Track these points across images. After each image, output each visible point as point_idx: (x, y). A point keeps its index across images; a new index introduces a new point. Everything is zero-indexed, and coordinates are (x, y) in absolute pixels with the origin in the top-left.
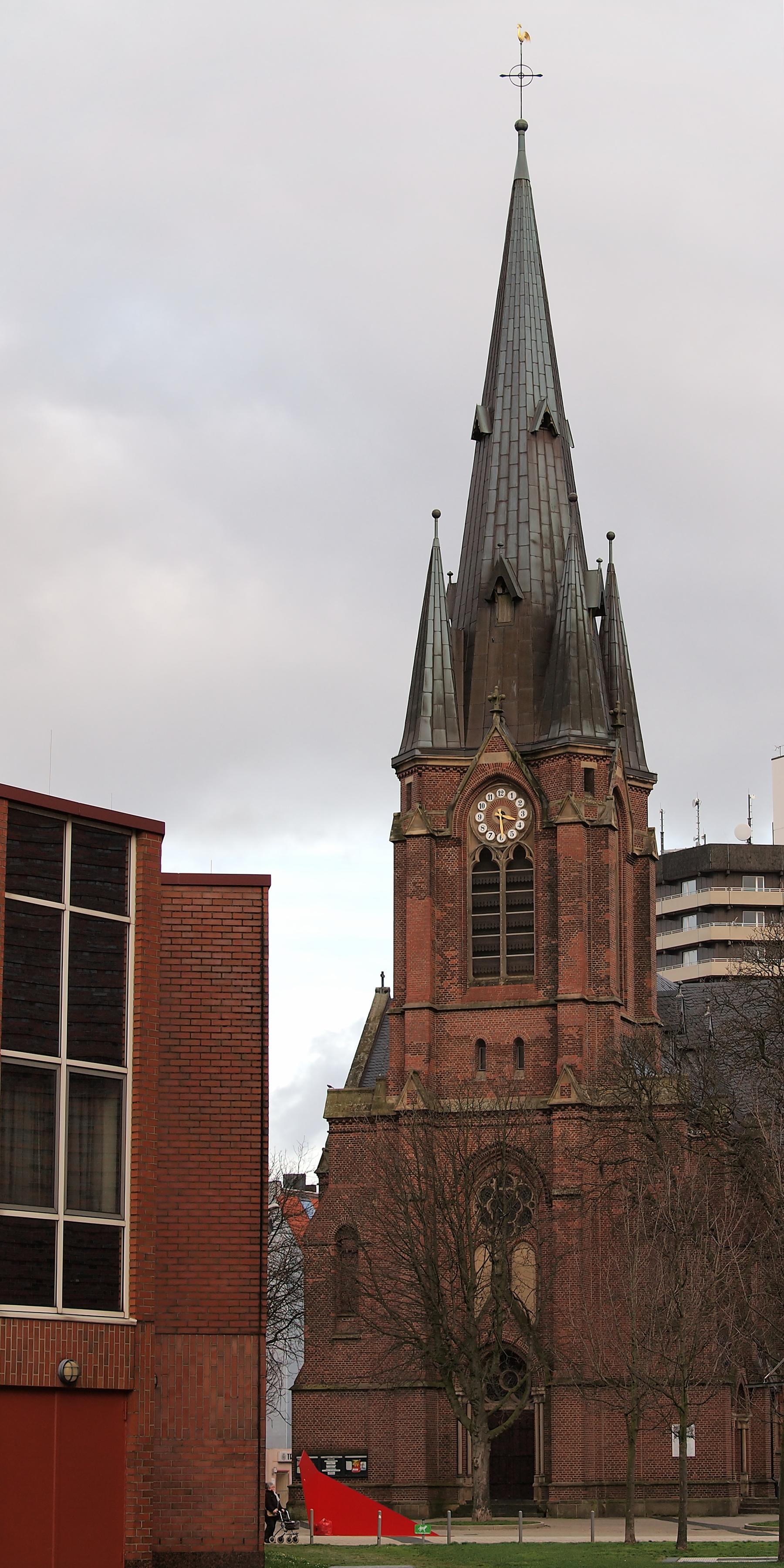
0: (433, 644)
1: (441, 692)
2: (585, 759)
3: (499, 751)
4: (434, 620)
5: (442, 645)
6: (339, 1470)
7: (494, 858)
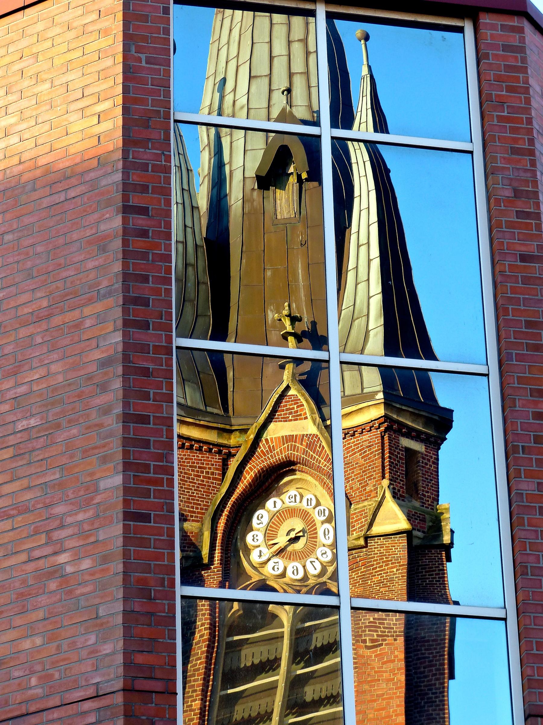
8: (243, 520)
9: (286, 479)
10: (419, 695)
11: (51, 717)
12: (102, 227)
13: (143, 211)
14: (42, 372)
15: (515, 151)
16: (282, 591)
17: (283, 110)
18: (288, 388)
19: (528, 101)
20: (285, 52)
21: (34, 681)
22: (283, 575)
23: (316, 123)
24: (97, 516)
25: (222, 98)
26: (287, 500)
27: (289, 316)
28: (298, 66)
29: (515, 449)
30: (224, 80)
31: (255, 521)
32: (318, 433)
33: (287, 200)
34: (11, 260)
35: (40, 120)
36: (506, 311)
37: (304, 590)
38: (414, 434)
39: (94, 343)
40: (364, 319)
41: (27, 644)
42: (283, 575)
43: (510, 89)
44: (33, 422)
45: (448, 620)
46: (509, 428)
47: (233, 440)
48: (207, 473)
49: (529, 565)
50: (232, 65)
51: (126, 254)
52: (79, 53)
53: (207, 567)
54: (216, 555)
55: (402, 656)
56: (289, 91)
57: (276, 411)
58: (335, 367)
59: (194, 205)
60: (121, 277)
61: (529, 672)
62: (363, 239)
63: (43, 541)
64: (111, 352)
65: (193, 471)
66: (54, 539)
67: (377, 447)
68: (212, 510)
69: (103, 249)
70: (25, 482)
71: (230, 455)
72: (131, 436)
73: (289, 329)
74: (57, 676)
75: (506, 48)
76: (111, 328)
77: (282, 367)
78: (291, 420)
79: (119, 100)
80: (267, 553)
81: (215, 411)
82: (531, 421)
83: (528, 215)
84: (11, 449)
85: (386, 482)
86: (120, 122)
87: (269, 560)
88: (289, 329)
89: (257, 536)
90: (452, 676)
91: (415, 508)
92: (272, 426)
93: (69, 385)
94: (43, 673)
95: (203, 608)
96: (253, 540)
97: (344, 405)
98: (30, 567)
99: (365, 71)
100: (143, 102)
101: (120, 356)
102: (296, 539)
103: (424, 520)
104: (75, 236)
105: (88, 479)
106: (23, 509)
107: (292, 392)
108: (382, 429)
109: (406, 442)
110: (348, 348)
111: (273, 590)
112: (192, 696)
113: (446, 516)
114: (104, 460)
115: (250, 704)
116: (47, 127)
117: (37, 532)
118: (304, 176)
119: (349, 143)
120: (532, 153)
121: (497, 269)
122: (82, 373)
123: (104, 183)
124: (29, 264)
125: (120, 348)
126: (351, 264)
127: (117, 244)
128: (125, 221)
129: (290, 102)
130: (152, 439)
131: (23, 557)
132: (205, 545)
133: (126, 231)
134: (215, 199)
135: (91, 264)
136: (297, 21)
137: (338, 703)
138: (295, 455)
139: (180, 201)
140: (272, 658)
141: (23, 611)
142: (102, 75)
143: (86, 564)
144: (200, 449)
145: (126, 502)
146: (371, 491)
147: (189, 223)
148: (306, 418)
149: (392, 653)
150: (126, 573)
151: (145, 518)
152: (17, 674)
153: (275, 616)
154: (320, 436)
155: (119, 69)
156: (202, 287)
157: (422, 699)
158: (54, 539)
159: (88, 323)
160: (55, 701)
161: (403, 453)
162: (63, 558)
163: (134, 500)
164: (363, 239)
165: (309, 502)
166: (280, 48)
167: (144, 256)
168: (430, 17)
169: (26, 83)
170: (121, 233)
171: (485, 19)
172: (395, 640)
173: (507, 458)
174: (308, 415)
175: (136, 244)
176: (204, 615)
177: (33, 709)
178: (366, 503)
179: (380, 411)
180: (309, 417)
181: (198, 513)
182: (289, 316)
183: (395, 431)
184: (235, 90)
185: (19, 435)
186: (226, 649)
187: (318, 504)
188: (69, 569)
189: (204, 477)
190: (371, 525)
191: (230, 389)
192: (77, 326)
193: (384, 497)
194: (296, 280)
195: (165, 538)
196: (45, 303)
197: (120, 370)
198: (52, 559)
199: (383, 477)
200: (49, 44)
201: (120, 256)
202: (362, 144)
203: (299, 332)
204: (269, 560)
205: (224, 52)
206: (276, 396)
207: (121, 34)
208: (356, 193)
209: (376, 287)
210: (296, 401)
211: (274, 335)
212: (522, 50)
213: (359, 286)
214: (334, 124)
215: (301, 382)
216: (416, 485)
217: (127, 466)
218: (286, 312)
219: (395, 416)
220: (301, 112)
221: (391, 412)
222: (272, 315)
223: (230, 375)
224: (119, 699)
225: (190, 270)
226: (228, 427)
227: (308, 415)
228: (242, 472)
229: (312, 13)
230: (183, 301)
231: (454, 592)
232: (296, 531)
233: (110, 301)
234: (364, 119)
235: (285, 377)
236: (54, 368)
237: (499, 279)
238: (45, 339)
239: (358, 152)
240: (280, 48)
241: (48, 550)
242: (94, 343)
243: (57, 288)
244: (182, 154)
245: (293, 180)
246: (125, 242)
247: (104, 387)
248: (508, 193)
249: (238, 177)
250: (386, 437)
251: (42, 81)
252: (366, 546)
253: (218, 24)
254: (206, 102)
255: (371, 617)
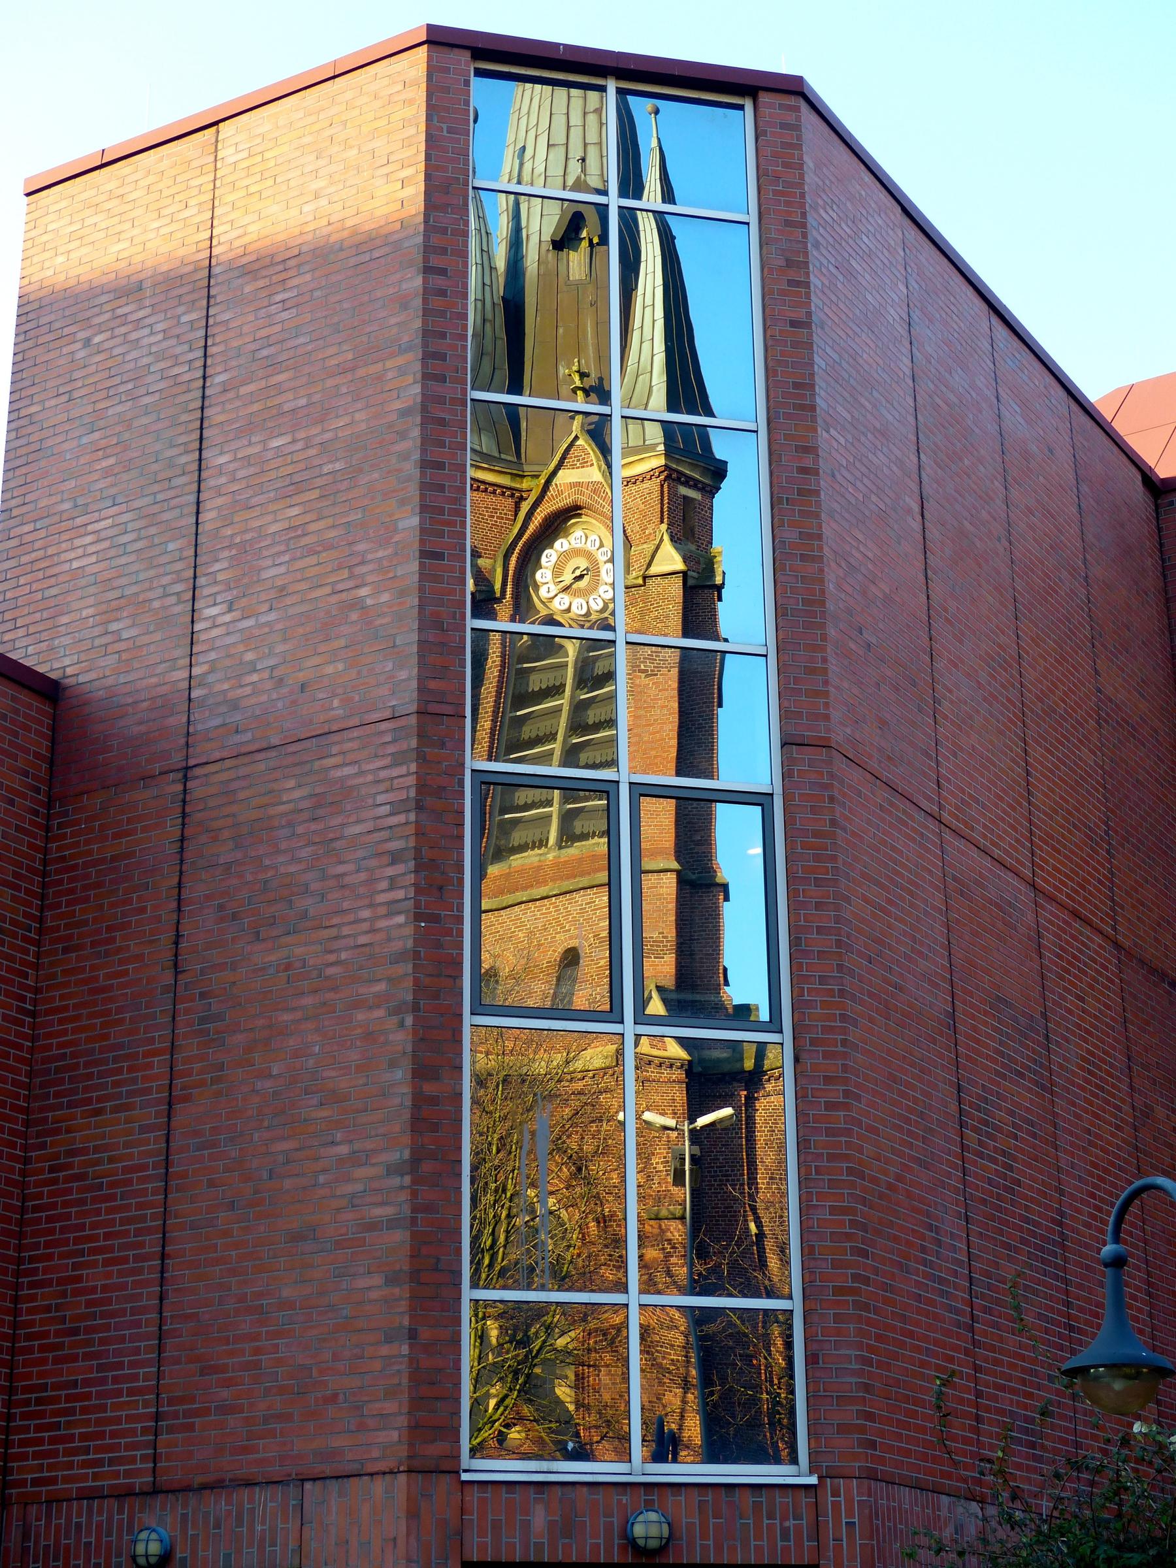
8: (533, 557)
9: (573, 521)
10: (691, 721)
11: (351, 736)
12: (404, 286)
13: (443, 272)
14: (347, 419)
15: (788, 223)
16: (567, 625)
17: (578, 178)
18: (576, 438)
19: (802, 176)
20: (580, 123)
21: (336, 703)
22: (568, 610)
23: (604, 192)
24: (396, 554)
25: (521, 165)
26: (573, 542)
27: (578, 372)
28: (592, 137)
29: (780, 500)
30: (524, 148)
31: (544, 559)
32: (603, 480)
33: (579, 263)
34: (319, 315)
35: (348, 184)
36: (775, 373)
37: (588, 625)
38: (691, 483)
39: (395, 394)
40: (649, 374)
41: (329, 669)
42: (568, 610)
43: (785, 165)
44: (338, 466)
45: (719, 656)
46: (775, 480)
47: (525, 484)
48: (501, 513)
49: (789, 607)
50: (532, 134)
51: (426, 312)
52: (384, 122)
53: (499, 601)
54: (508, 590)
55: (676, 685)
56: (583, 160)
57: (565, 459)
58: (617, 422)
59: (493, 266)
60: (420, 333)
61: (786, 704)
62: (649, 301)
63: (346, 576)
64: (411, 403)
65: (487, 512)
66: (356, 573)
67: (656, 494)
68: (504, 548)
69: (405, 307)
70: (330, 521)
71: (522, 499)
72: (428, 481)
73: (578, 383)
74: (357, 698)
75: (784, 126)
76: (411, 381)
77: (572, 418)
78: (578, 468)
79: (422, 167)
80: (554, 590)
81: (509, 458)
82: (796, 475)
83: (798, 284)
84: (318, 491)
85: (664, 527)
86: (422, 188)
87: (556, 595)
88: (578, 383)
90: (720, 705)
91: (691, 551)
92: (561, 473)
93: (372, 432)
94: (344, 696)
95: (495, 638)
97: (624, 456)
98: (334, 599)
99: (654, 143)
100: (445, 169)
101: (419, 407)
102: (581, 577)
103: (698, 563)
104: (379, 294)
105: (388, 520)
106: (328, 546)
107: (580, 442)
108: (662, 477)
109: (684, 491)
110: (632, 405)
111: (560, 624)
112: (484, 717)
113: (718, 559)
114: (403, 502)
115: (538, 725)
116: (354, 191)
117: (340, 568)
118: (596, 240)
119: (638, 212)
120: (804, 225)
121: (769, 333)
122: (384, 421)
123: (406, 245)
124: (336, 319)
125: (419, 399)
126: (637, 324)
127: (418, 302)
128: (425, 281)
129: (584, 170)
130: (447, 484)
131: (328, 590)
133: (426, 291)
134: (511, 262)
135: (393, 321)
136: (593, 96)
137: (612, 726)
138: (583, 499)
139: (479, 261)
140: (557, 684)
141: (327, 639)
142: (406, 143)
143: (385, 597)
144: (494, 492)
145: (422, 542)
146: (650, 534)
147: (487, 281)
148: (592, 465)
149: (666, 682)
150: (421, 607)
151: (439, 556)
152: (321, 696)
153: (561, 647)
154: (604, 483)
155: (423, 137)
156: (499, 343)
157: (692, 725)
158: (356, 573)
159: (390, 375)
160: (355, 721)
161: (680, 501)
162: (363, 592)
163: (430, 541)
164: (649, 301)
166: (576, 119)
167: (443, 314)
168: (713, 94)
169: (336, 148)
170: (421, 291)
171: (764, 98)
172: (669, 671)
173: (772, 509)
174: (594, 462)
175: (437, 302)
176: (495, 644)
177: (335, 728)
178: (645, 546)
179: (661, 461)
180: (595, 464)
181: (492, 550)
182: (578, 372)
183: (674, 480)
184: (534, 157)
185: (325, 477)
186: (516, 674)
187: (602, 546)
188: (369, 602)
189: (498, 517)
190: (649, 565)
191: (523, 438)
192: (379, 378)
193: (662, 540)
194: (586, 338)
195: (457, 575)
196: (350, 356)
197: (418, 420)
198: (354, 592)
199: (662, 522)
200: (356, 112)
201: (420, 313)
202: (650, 214)
203: (587, 387)
204: (556, 595)
205: (524, 121)
206: (565, 446)
207: (424, 104)
208: (643, 258)
209: (660, 346)
210: (584, 450)
211: (565, 390)
212: (797, 128)
213: (643, 345)
214: (623, 193)
215: (589, 432)
216: (692, 530)
217: (424, 508)
218: (575, 368)
219: (674, 466)
220: (595, 182)
221: (671, 462)
222: (563, 371)
223: (524, 425)
224: (413, 720)
225: (488, 325)
226: (521, 473)
227: (594, 462)
228: (533, 514)
229: (602, 89)
230: (480, 354)
231: (724, 628)
232: (581, 569)
233: (410, 356)
234: (652, 189)
235: (574, 428)
236: (358, 416)
237: (770, 343)
238: (351, 389)
239: (646, 220)
240: (576, 119)
241: (351, 584)
242: (395, 394)
243: (362, 342)
244: (481, 218)
245: (585, 244)
246: (425, 301)
247: (403, 435)
248: (782, 263)
249: (534, 240)
250: (666, 486)
251: (351, 147)
252: (644, 585)
253: (520, 93)
254: (506, 169)
255: (648, 650)
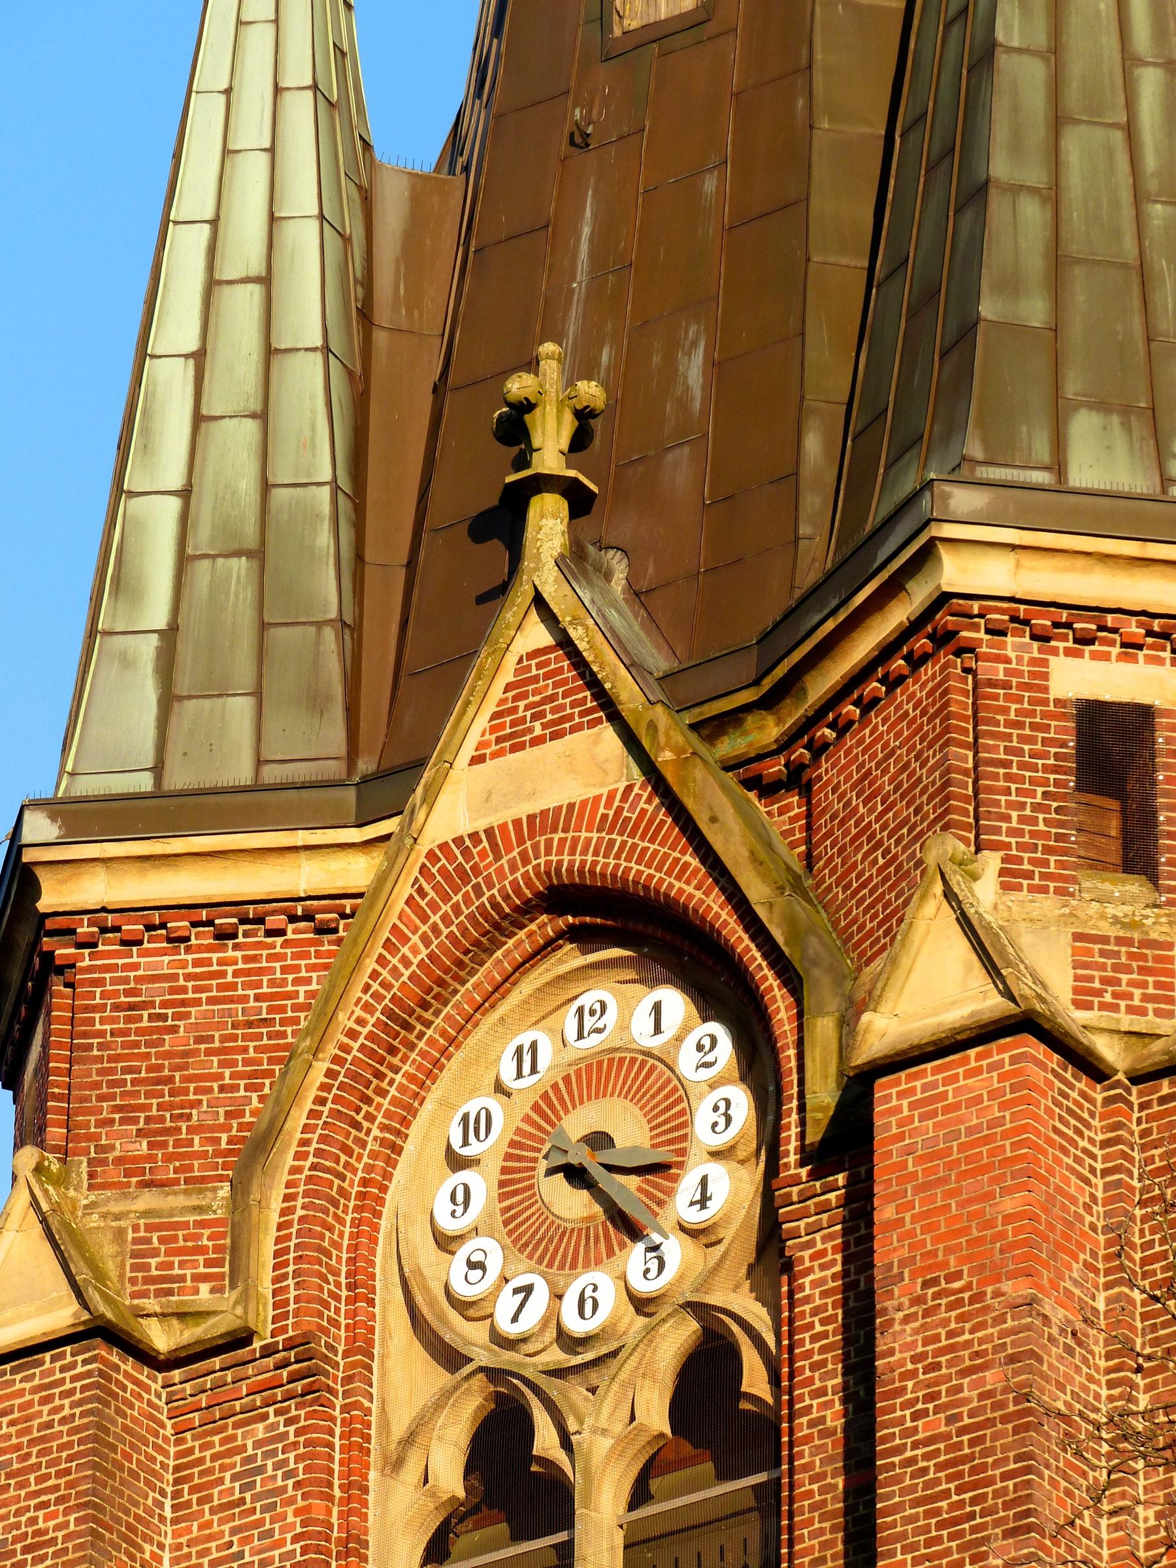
0: (214, 223)
1: (247, 485)
2: (1085, 640)
3: (555, 736)
4: (272, 150)
5: (272, 219)
6: (1171, 1274)
7: (545, 1441)
78: (537, 741)
89: (453, 1213)
96: (728, 1103)
132: (825, 1065)
165: (527, 1059)
